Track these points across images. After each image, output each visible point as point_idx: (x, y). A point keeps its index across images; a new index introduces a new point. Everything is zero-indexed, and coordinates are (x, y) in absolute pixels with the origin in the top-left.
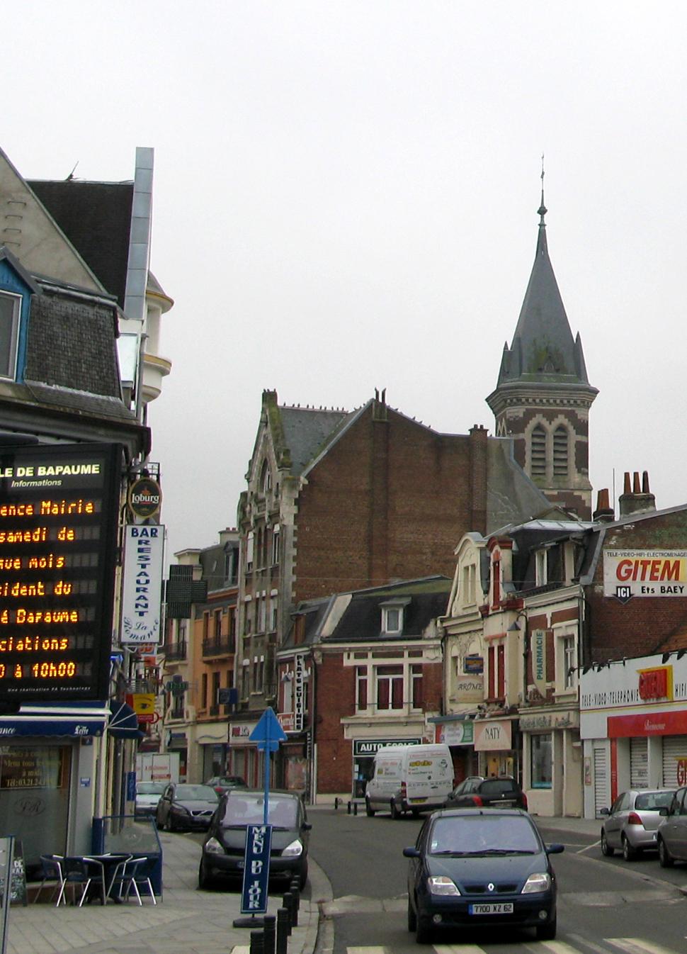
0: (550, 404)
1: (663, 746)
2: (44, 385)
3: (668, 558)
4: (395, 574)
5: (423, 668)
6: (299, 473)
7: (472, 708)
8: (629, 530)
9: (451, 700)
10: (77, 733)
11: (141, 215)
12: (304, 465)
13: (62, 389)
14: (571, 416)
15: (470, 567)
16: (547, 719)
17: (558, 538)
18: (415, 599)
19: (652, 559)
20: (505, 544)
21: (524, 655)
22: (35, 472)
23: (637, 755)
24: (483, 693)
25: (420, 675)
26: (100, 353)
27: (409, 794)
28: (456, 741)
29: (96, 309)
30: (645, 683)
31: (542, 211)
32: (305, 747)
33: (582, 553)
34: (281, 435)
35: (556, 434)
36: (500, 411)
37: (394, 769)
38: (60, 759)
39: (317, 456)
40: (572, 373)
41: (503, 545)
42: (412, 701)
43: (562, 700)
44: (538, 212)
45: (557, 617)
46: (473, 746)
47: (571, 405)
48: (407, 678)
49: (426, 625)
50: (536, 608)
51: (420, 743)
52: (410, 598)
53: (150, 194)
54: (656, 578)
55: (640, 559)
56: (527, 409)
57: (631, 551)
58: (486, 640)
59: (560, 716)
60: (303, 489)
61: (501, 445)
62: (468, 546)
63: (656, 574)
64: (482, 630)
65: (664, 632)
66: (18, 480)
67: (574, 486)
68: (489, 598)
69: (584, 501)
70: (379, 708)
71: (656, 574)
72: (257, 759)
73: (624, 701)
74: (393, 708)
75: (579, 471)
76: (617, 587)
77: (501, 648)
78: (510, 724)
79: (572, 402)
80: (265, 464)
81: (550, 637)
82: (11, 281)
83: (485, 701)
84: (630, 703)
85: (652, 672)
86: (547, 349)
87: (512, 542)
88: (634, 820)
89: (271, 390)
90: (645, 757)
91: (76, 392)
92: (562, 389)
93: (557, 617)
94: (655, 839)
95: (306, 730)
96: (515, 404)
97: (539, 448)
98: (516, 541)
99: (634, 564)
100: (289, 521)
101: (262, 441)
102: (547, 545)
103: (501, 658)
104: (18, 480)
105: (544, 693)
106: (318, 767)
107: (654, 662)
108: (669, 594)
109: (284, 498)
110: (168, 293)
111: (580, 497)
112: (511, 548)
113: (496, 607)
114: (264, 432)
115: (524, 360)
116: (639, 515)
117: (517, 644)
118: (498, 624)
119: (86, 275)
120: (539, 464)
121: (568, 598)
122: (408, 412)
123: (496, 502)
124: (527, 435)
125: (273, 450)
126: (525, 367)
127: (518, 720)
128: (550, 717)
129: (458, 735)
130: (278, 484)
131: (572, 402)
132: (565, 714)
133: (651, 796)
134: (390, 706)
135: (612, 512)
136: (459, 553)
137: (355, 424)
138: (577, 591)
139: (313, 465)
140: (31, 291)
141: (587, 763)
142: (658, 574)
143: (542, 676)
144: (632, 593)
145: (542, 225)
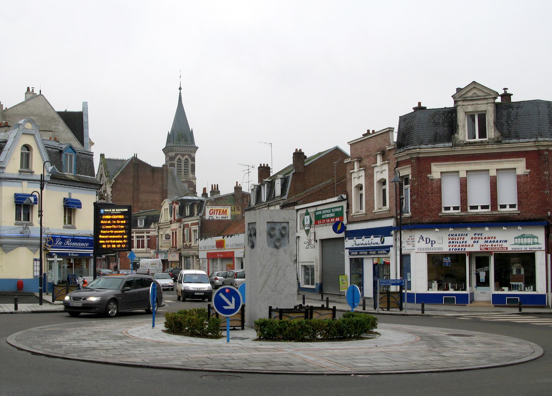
0: (181, 152)
2: (80, 175)
3: (224, 209)
4: (141, 209)
6: (112, 179)
7: (167, 249)
11: (86, 121)
12: (113, 176)
13: (83, 176)
14: (190, 155)
17: (193, 202)
18: (148, 217)
19: (219, 209)
20: (177, 203)
24: (171, 245)
31: (180, 89)
32: (116, 259)
33: (200, 207)
37: (146, 265)
43: (193, 248)
44: (179, 89)
45: (192, 224)
46: (168, 260)
47: (190, 152)
48: (146, 240)
49: (151, 224)
53: (88, 115)
54: (220, 214)
55: (216, 209)
58: (171, 230)
62: (165, 203)
75: (192, 173)
77: (176, 232)
78: (178, 254)
80: (101, 175)
81: (190, 230)
82: (72, 151)
86: (182, 134)
88: (216, 279)
89: (103, 154)
90: (217, 263)
91: (86, 176)
92: (187, 147)
93: (192, 224)
94: (222, 284)
96: (172, 152)
97: (179, 166)
103: (176, 235)
105: (188, 245)
107: (220, 238)
108: (224, 219)
110: (93, 142)
111: (192, 181)
112: (178, 204)
114: (101, 166)
115: (175, 137)
116: (216, 196)
118: (175, 226)
120: (179, 171)
121: (195, 219)
123: (170, 187)
124: (175, 162)
126: (175, 140)
132: (194, 251)
135: (207, 194)
138: (198, 217)
139: (116, 176)
140: (76, 153)
141: (201, 265)
142: (221, 213)
145: (180, 93)
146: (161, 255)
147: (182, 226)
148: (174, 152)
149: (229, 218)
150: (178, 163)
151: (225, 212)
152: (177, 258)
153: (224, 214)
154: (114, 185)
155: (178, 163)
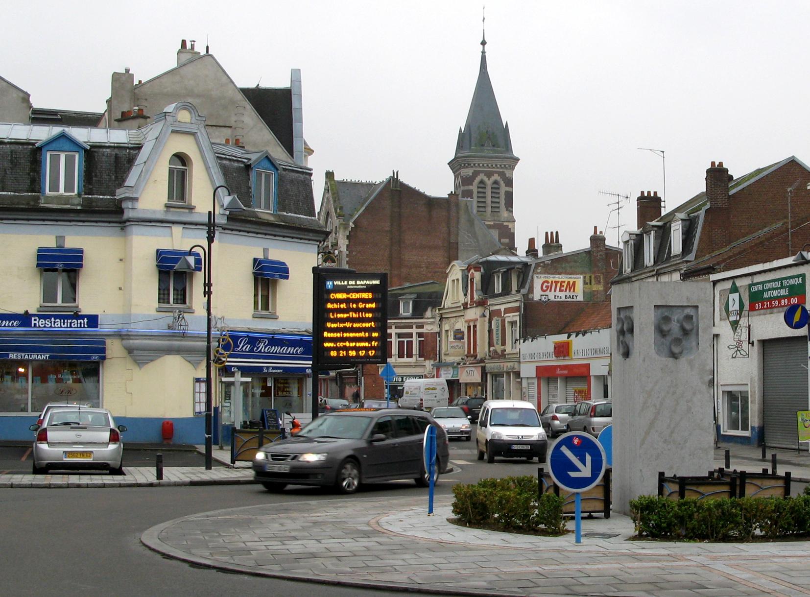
1: (566, 382)
2: (285, 214)
3: (569, 280)
4: (407, 279)
5: (424, 335)
6: (348, 221)
7: (457, 359)
8: (548, 264)
9: (445, 354)
10: (233, 370)
12: (351, 216)
13: (292, 215)
14: (502, 175)
15: (456, 281)
16: (502, 366)
18: (419, 295)
19: (560, 280)
20: (477, 269)
21: (488, 331)
22: (356, 282)
23: (552, 387)
24: (465, 350)
25: (423, 339)
26: (307, 196)
27: (424, 405)
28: (448, 377)
29: (304, 175)
30: (557, 349)
31: (484, 43)
32: (357, 378)
33: (522, 276)
34: (337, 198)
35: (492, 186)
36: (457, 171)
38: (298, 383)
39: (359, 210)
40: (503, 148)
41: (476, 269)
42: (418, 353)
43: (509, 356)
45: (507, 311)
46: (458, 380)
47: (502, 168)
48: (415, 340)
49: (426, 310)
50: (495, 305)
51: (423, 378)
52: (416, 295)
54: (562, 291)
55: (554, 280)
56: (475, 171)
57: (549, 276)
58: (466, 321)
59: (510, 365)
60: (352, 230)
61: (466, 203)
62: (454, 268)
63: (562, 288)
64: (464, 315)
65: (566, 320)
66: (350, 285)
67: (504, 219)
68: (467, 299)
69: (510, 229)
70: (399, 357)
71: (562, 288)
72: (327, 385)
73: (546, 357)
74: (407, 357)
75: (507, 210)
76: (541, 295)
77: (475, 326)
79: (503, 166)
80: (328, 214)
81: (503, 321)
82: (269, 166)
83: (466, 355)
84: (549, 359)
85: (561, 343)
87: (481, 268)
88: (555, 418)
89: (331, 171)
90: (556, 388)
93: (507, 311)
94: (565, 428)
95: (357, 369)
96: (467, 167)
97: (482, 195)
98: (483, 267)
99: (550, 282)
100: (344, 249)
101: (326, 200)
102: (501, 271)
103: (475, 332)
104: (350, 285)
105: (500, 352)
106: (364, 390)
107: (563, 338)
108: (570, 300)
109: (340, 235)
112: (480, 271)
113: (472, 304)
114: (327, 196)
115: (472, 139)
116: (553, 255)
117: (484, 325)
118: (473, 313)
119: (277, 143)
120: (482, 204)
121: (514, 300)
122: (412, 184)
123: (464, 238)
124: (474, 188)
125: (333, 207)
126: (473, 144)
127: (485, 366)
128: (503, 365)
129: (450, 373)
130: (336, 227)
131: (503, 166)
132: (512, 364)
133: (562, 407)
134: (405, 356)
135: (537, 251)
136: (449, 272)
137: (381, 194)
138: (519, 297)
140: (277, 169)
141: (524, 390)
142: (564, 288)
143: (499, 342)
144: (549, 298)
145: (483, 52)
146: (445, 371)
147: (487, 314)
148: (472, 167)
149: (580, 298)
150: (480, 190)
151: (572, 286)
152: (476, 377)
153: (570, 291)
154: (352, 234)
155: (480, 190)
